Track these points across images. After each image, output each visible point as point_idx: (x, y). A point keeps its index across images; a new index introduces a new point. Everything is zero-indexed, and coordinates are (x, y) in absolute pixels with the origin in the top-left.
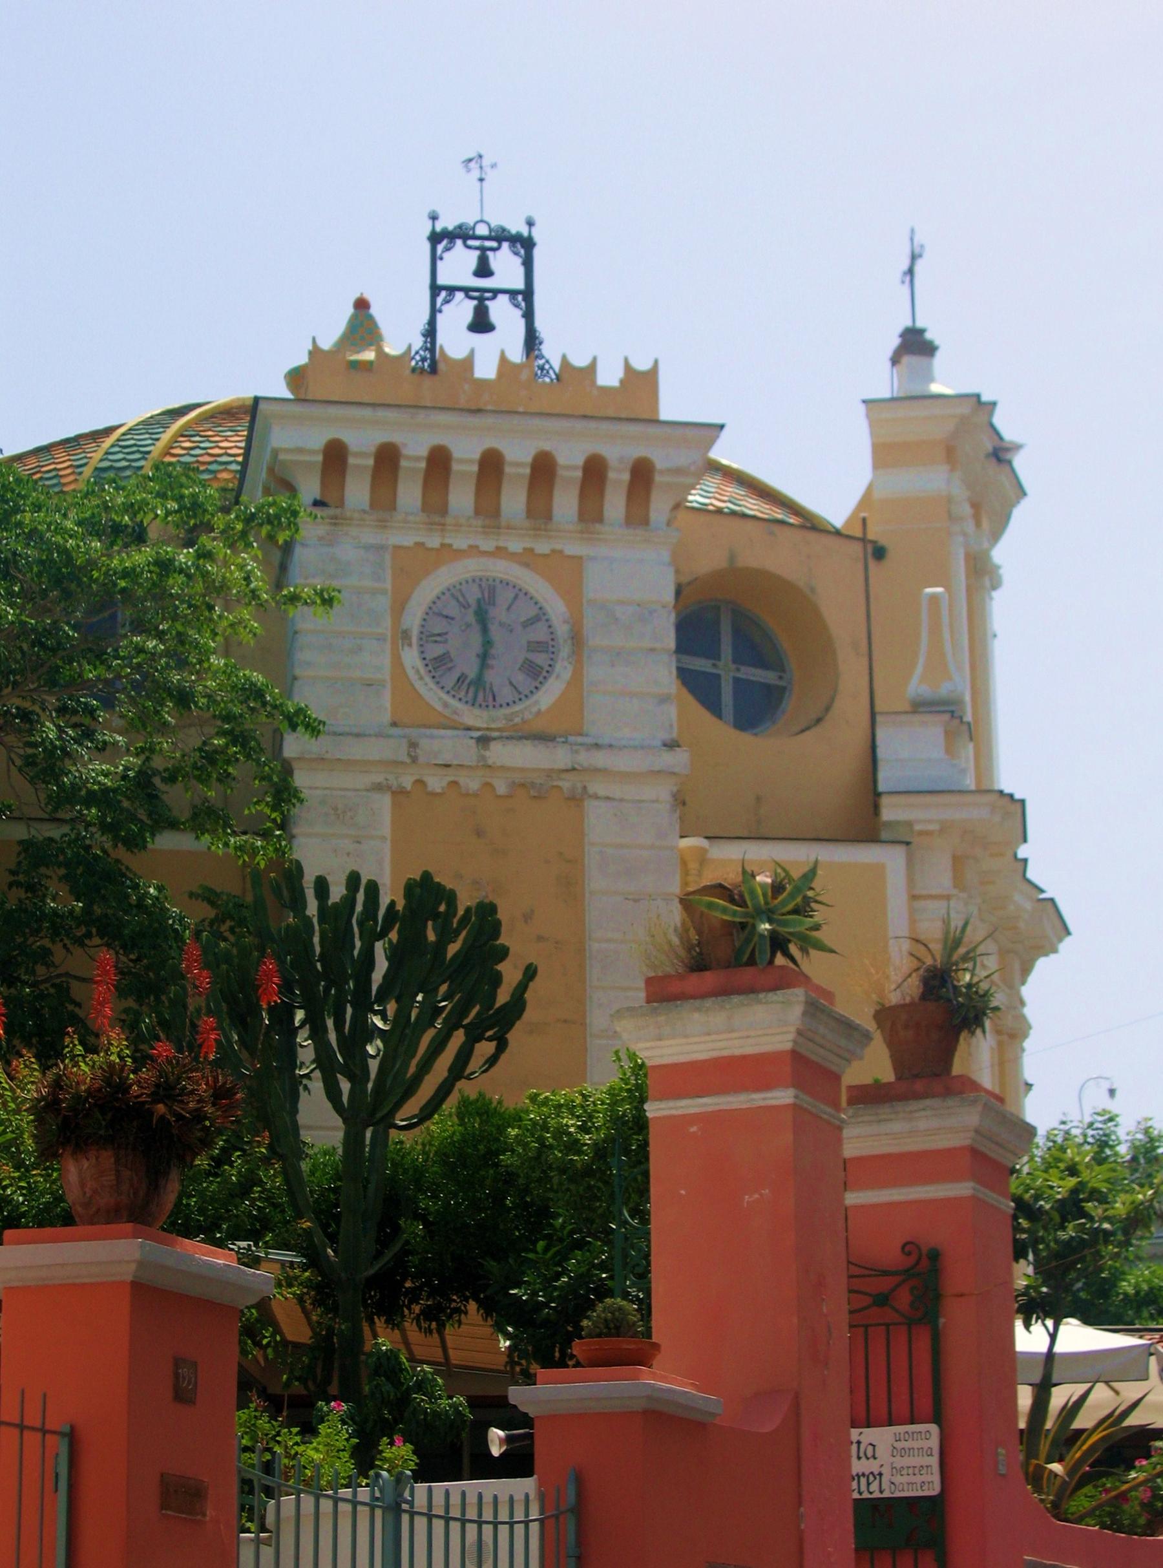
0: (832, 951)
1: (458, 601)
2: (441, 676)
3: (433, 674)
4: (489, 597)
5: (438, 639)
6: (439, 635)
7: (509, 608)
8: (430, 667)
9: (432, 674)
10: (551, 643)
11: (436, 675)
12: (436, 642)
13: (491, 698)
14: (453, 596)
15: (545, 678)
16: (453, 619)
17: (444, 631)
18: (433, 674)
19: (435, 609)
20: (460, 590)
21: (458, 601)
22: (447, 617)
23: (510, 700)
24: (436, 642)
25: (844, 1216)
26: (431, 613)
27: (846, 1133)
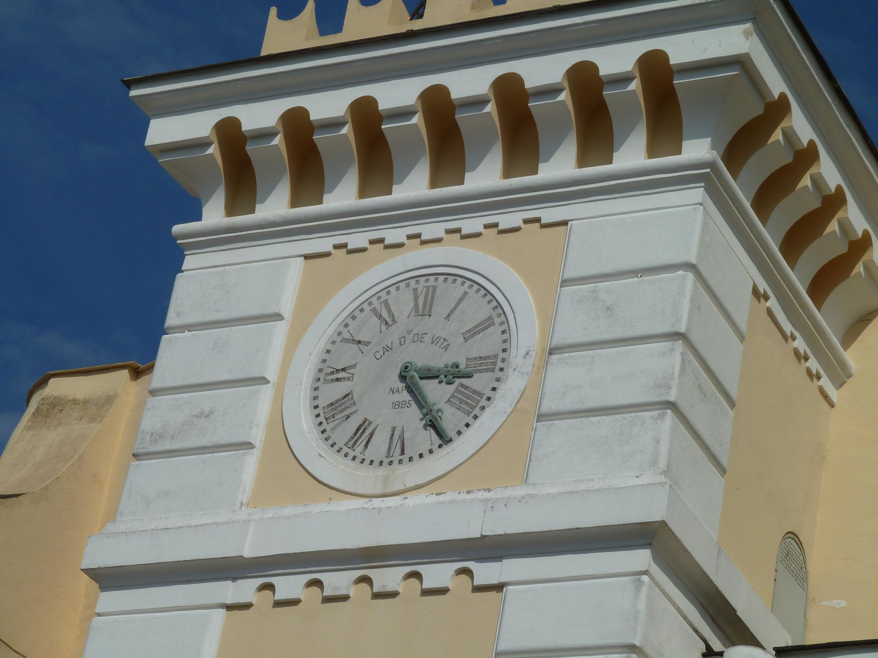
0: (20, 495)
1: (381, 317)
2: (333, 429)
3: (352, 454)
4: (424, 306)
5: (342, 375)
6: (343, 370)
7: (448, 317)
8: (322, 419)
9: (350, 457)
10: (502, 355)
11: (328, 427)
12: (338, 380)
13: (398, 451)
14: (374, 310)
15: (483, 408)
16: (367, 343)
17: (353, 363)
18: (352, 454)
19: (347, 335)
20: (386, 303)
21: (381, 317)
22: (359, 342)
23: (424, 450)
24: (338, 380)
25: (330, 327)
26: (405, 458)
27: (190, 261)
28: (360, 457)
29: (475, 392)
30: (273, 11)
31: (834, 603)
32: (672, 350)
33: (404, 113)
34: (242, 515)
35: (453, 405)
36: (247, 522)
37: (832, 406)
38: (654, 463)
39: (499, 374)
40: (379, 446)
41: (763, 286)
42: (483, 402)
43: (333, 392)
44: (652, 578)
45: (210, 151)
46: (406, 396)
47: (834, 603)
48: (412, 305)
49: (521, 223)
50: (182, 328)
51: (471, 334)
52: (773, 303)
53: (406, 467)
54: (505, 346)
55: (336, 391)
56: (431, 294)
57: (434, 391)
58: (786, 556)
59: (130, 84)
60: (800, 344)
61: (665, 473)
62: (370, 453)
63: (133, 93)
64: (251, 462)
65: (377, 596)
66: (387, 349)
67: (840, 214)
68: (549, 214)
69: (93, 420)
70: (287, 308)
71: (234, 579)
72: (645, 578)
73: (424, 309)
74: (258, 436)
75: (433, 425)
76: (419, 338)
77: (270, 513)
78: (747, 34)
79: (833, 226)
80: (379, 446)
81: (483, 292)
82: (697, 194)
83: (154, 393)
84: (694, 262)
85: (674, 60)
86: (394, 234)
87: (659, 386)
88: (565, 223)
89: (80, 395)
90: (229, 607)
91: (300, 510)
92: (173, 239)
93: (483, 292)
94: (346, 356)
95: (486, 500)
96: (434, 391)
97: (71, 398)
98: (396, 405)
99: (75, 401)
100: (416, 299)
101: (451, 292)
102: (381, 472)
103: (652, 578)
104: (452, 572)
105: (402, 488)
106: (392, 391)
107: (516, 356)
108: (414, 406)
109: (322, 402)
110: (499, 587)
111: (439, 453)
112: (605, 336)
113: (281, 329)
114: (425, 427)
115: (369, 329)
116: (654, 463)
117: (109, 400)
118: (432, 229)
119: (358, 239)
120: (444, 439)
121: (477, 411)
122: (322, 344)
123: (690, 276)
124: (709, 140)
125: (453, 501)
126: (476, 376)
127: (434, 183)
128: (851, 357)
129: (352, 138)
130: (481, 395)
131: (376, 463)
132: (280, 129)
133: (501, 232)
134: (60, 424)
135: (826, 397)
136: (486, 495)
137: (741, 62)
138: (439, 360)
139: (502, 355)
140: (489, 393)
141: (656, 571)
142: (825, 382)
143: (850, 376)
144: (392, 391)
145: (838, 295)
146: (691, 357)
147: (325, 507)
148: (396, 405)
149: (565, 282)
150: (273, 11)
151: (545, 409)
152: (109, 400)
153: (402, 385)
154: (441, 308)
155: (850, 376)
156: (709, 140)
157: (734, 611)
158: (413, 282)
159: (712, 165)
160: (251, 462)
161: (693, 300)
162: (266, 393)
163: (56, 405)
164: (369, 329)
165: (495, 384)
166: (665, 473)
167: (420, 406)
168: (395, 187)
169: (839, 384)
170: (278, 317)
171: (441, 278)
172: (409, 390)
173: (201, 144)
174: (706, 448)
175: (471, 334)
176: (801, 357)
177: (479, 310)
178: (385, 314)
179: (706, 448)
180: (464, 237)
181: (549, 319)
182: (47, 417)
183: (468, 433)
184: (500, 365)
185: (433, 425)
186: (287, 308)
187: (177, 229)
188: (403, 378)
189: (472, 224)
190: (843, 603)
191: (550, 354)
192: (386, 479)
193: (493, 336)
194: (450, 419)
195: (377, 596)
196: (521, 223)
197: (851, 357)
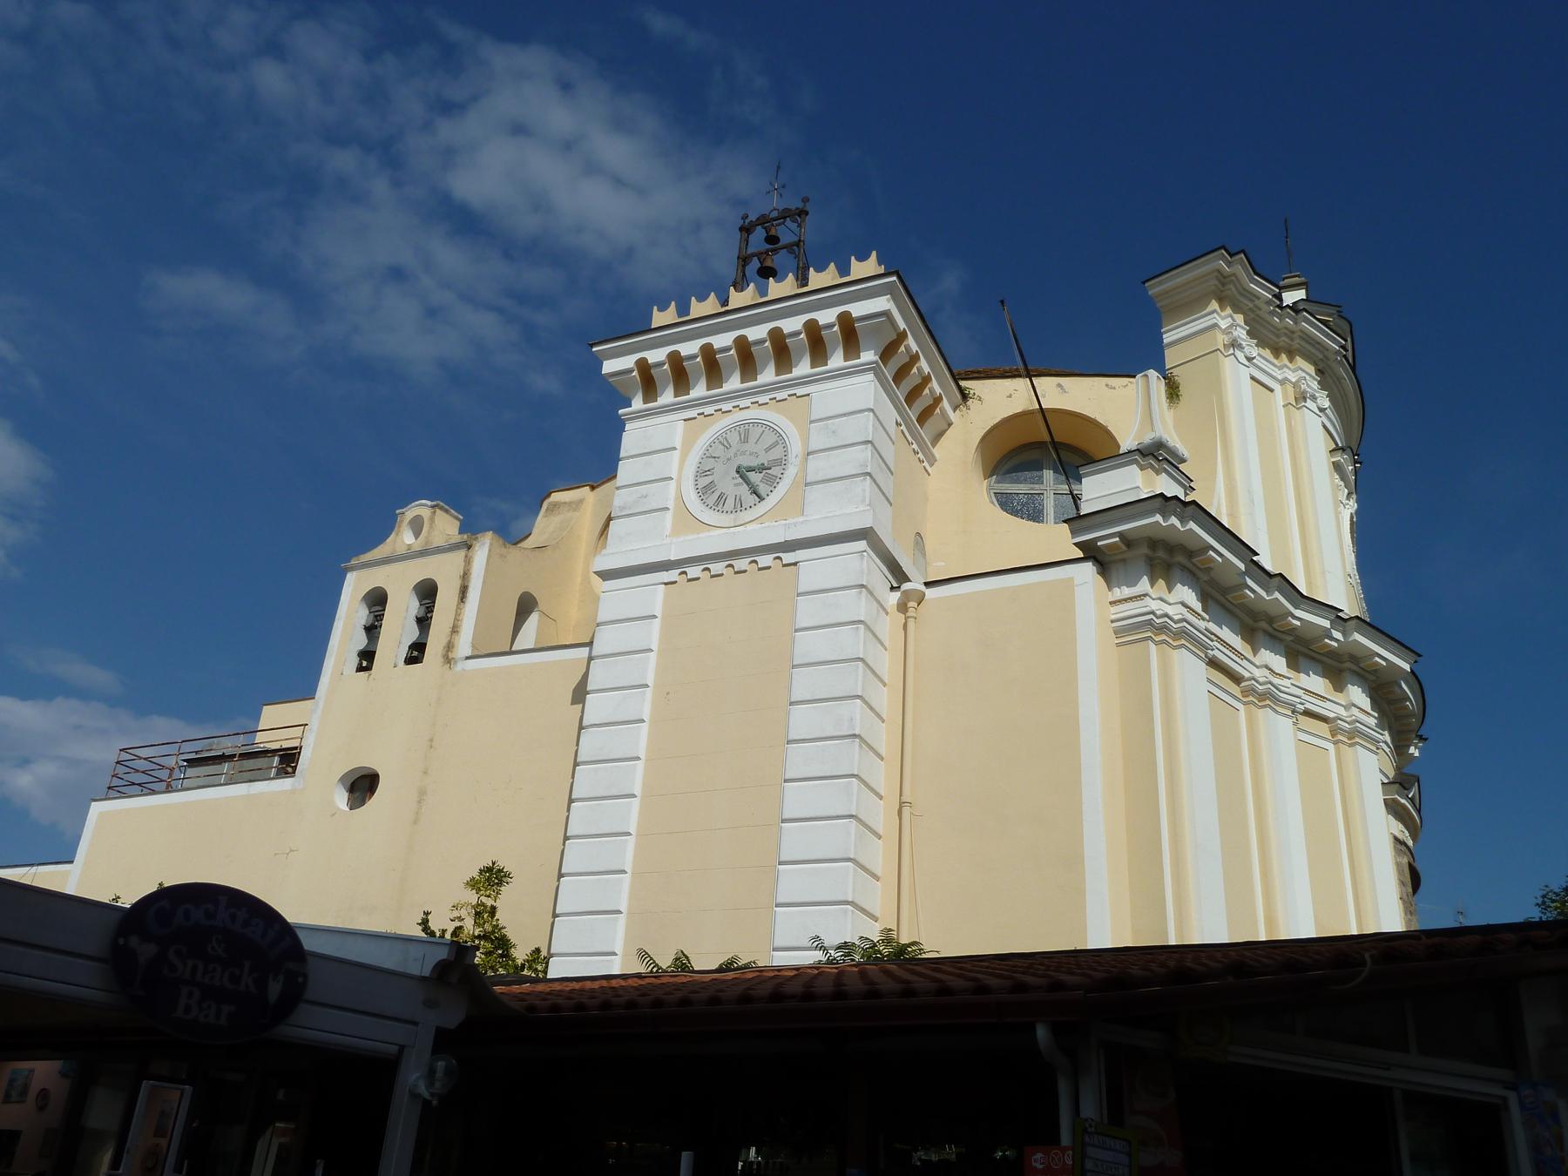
7: (756, 443)
8: (700, 494)
10: (784, 458)
14: (720, 442)
16: (718, 458)
20: (726, 438)
28: (721, 510)
29: (773, 476)
30: (655, 308)
31: (939, 564)
32: (866, 449)
33: (727, 349)
34: (668, 540)
35: (764, 482)
36: (671, 543)
37: (929, 475)
38: (863, 501)
39: (784, 467)
40: (730, 503)
41: (899, 420)
42: (778, 480)
43: (704, 481)
44: (869, 555)
45: (634, 374)
46: (740, 480)
47: (939, 564)
48: (738, 438)
49: (787, 397)
50: (628, 458)
51: (768, 450)
52: (903, 427)
53: (744, 512)
54: (786, 453)
55: (707, 480)
56: (747, 433)
57: (752, 476)
58: (917, 543)
59: (592, 346)
60: (915, 446)
61: (869, 505)
62: (725, 509)
63: (594, 349)
64: (669, 515)
65: (736, 573)
66: (728, 460)
67: (929, 385)
68: (800, 391)
69: (575, 510)
70: (678, 444)
71: (667, 571)
72: (865, 554)
73: (745, 439)
74: (671, 505)
75: (755, 493)
76: (743, 453)
77: (681, 539)
78: (888, 300)
79: (927, 391)
80: (730, 503)
81: (772, 430)
82: (870, 376)
83: (618, 488)
84: (872, 407)
85: (650, 361)
86: (726, 406)
87: (861, 466)
88: (808, 395)
89: (567, 500)
90: (666, 584)
91: (696, 536)
92: (619, 417)
93: (772, 430)
94: (710, 464)
95: (786, 525)
96: (752, 476)
97: (563, 501)
98: (736, 485)
99: (565, 503)
100: (740, 435)
101: (755, 432)
102: (732, 516)
103: (869, 555)
104: (772, 559)
105: (743, 522)
106: (733, 478)
107: (791, 457)
108: (745, 485)
109: (700, 487)
110: (795, 564)
111: (759, 505)
112: (834, 445)
113: (676, 454)
114: (751, 493)
115: (719, 450)
116: (863, 501)
117: (581, 501)
118: (744, 403)
119: (709, 410)
120: (761, 498)
121: (775, 484)
122: (697, 459)
123: (872, 414)
124: (873, 352)
125: (769, 526)
126: (773, 468)
127: (709, 389)
128: (936, 451)
129: (805, 339)
130: (776, 477)
131: (753, 506)
132: (733, 346)
133: (777, 401)
134: (559, 513)
135: (926, 471)
136: (784, 522)
137: (886, 314)
138: (755, 463)
139: (784, 458)
140: (780, 476)
141: (869, 550)
142: (926, 464)
143: (936, 461)
144: (733, 478)
145: (930, 423)
146: (874, 451)
147: (707, 534)
148: (736, 485)
149: (811, 422)
150: (655, 308)
151: (808, 481)
152: (581, 501)
153: (738, 476)
154: (752, 439)
155: (936, 461)
156: (873, 352)
157: (901, 568)
158: (738, 428)
159: (876, 362)
160: (669, 515)
161: (873, 426)
162: (673, 484)
163: (556, 505)
164: (719, 450)
165: (783, 471)
166: (869, 505)
167: (748, 485)
168: (758, 376)
169: (931, 465)
170: (675, 449)
171: (751, 425)
172: (741, 477)
173: (631, 371)
174: (883, 494)
175: (768, 450)
176: (916, 453)
177: (770, 438)
178: (726, 444)
179: (883, 494)
180: (760, 405)
181: (806, 439)
182: (552, 511)
183: (772, 495)
184: (784, 462)
185: (755, 493)
186: (678, 444)
187: (620, 412)
188: (738, 472)
189: (763, 399)
190: (943, 564)
191: (808, 455)
192: (735, 520)
193: (779, 448)
194: (763, 489)
195: (736, 573)
196: (787, 397)
197: (936, 451)
